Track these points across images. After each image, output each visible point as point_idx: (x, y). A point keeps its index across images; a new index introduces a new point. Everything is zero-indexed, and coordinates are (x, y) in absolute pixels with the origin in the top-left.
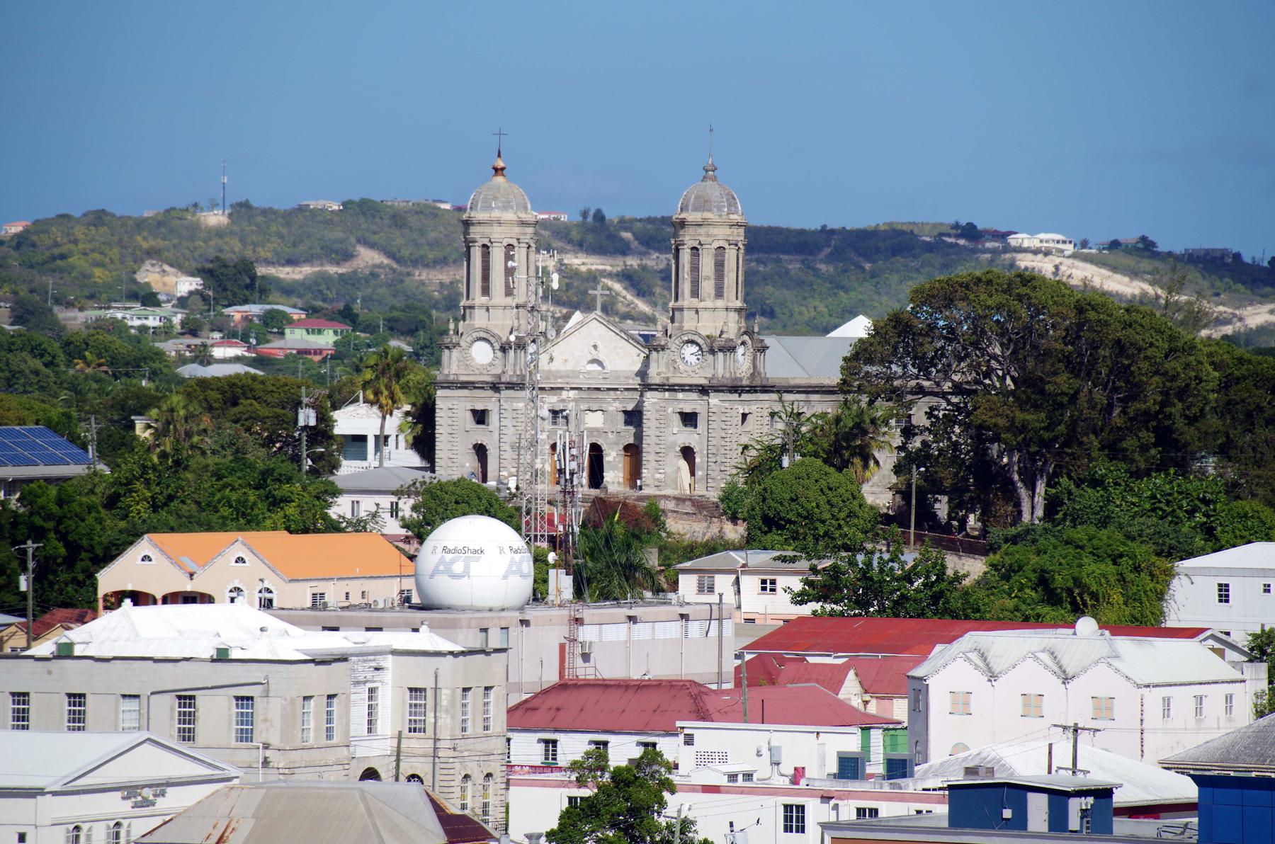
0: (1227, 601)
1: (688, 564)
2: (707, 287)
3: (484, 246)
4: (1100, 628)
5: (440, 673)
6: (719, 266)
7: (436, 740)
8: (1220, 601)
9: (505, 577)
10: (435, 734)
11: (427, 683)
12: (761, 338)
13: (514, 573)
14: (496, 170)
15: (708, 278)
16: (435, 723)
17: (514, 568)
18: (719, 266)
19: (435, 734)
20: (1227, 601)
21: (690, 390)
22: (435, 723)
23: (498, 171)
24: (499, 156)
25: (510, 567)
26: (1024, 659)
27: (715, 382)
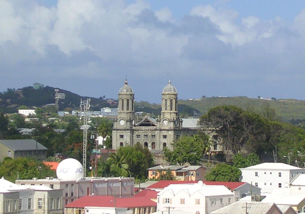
0: (281, 176)
1: (150, 169)
2: (169, 108)
3: (123, 100)
4: (203, 183)
5: (45, 195)
6: (171, 104)
7: (44, 210)
8: (279, 176)
9: (76, 173)
10: (44, 209)
11: (43, 198)
12: (182, 119)
13: (78, 171)
14: (125, 83)
15: (168, 106)
16: (44, 207)
17: (78, 171)
18: (171, 104)
19: (44, 209)
20: (281, 176)
21: (165, 130)
22: (44, 207)
23: (126, 83)
24: (126, 80)
25: (77, 170)
26: (181, 191)
27: (170, 129)
